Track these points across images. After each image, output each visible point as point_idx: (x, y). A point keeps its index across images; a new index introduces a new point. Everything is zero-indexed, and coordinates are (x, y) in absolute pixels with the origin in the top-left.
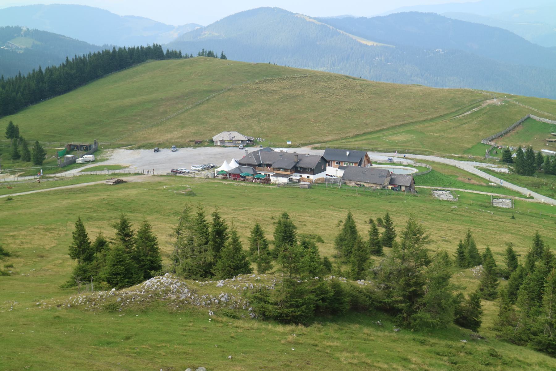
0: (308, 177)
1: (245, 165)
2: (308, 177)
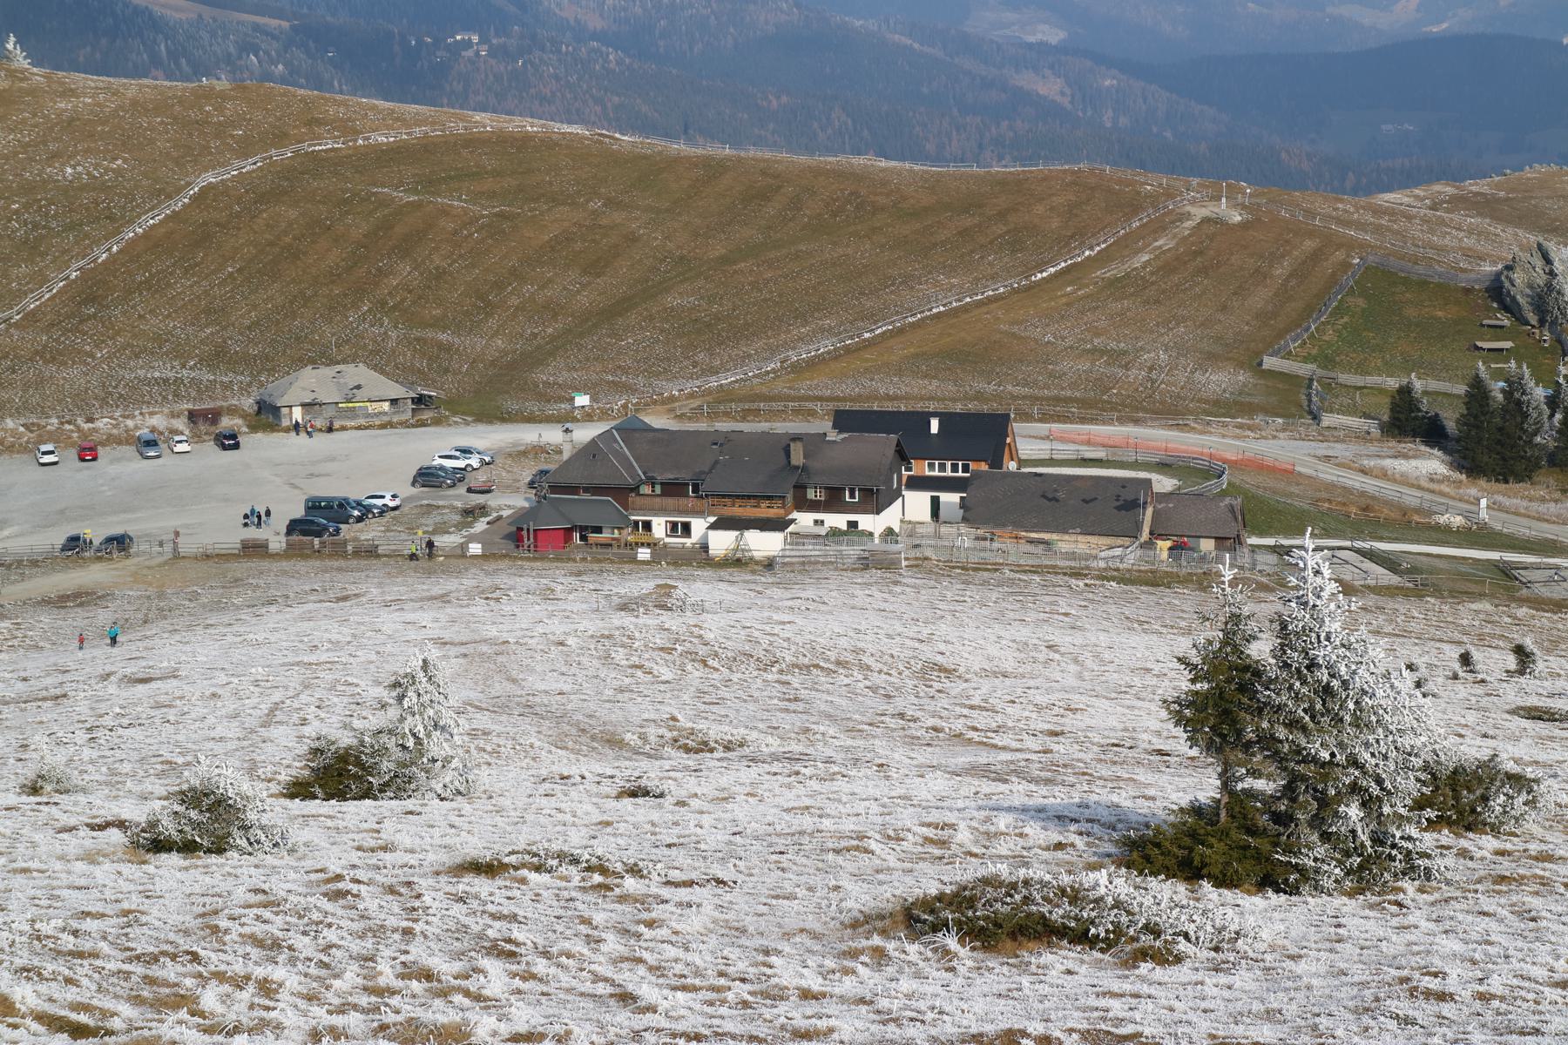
0: (853, 525)
1: (573, 490)
2: (853, 525)
